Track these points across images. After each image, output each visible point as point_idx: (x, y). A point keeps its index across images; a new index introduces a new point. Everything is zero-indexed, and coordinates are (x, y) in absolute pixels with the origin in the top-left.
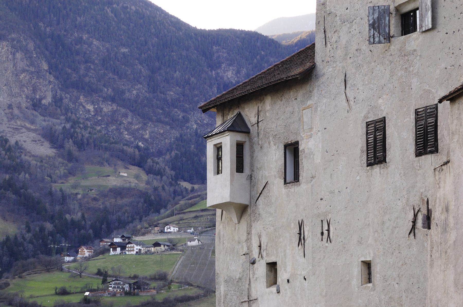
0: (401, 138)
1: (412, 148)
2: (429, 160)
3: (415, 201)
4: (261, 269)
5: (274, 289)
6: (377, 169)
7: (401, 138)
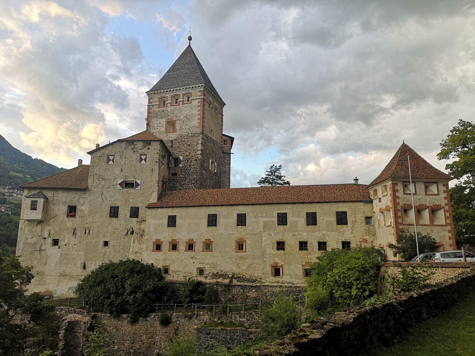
0: (124, 212)
1: (128, 215)
2: (135, 220)
3: (128, 227)
4: (50, 241)
5: (57, 247)
6: (114, 219)
7: (124, 212)
